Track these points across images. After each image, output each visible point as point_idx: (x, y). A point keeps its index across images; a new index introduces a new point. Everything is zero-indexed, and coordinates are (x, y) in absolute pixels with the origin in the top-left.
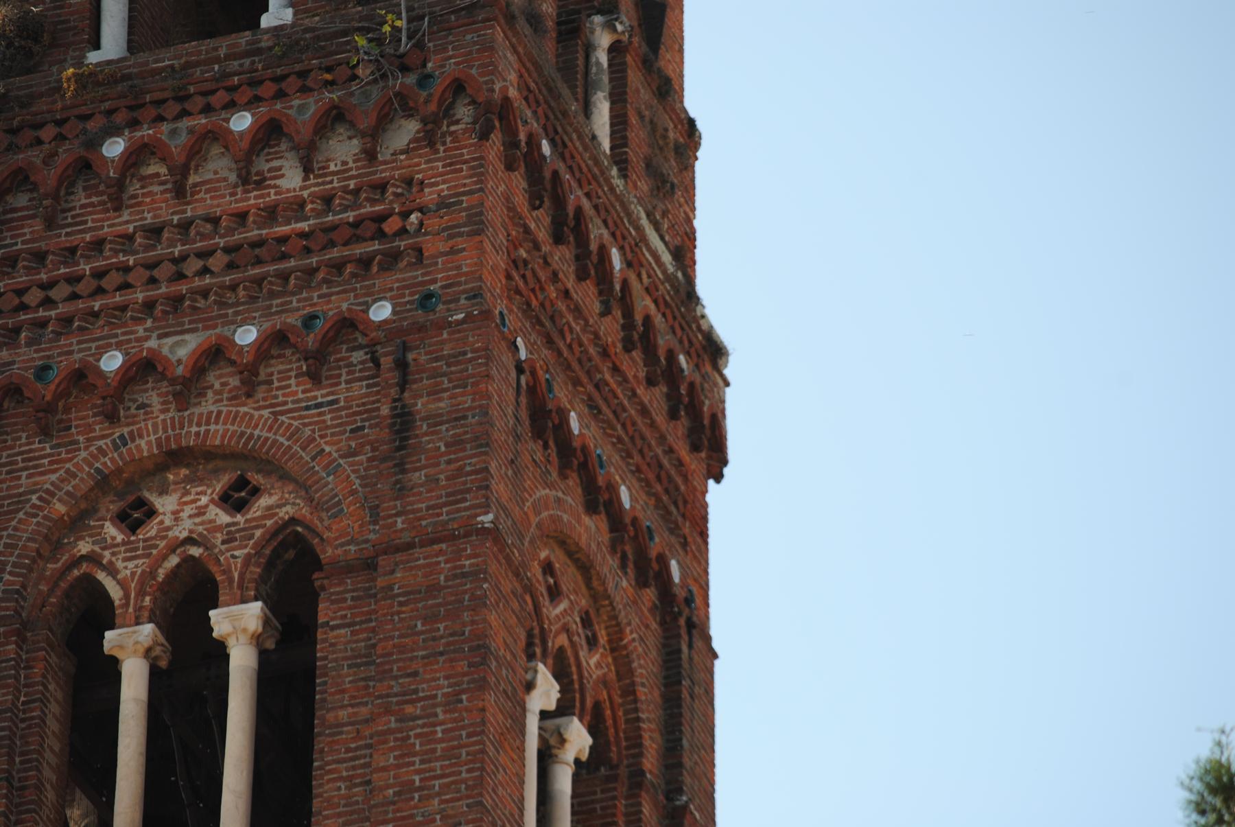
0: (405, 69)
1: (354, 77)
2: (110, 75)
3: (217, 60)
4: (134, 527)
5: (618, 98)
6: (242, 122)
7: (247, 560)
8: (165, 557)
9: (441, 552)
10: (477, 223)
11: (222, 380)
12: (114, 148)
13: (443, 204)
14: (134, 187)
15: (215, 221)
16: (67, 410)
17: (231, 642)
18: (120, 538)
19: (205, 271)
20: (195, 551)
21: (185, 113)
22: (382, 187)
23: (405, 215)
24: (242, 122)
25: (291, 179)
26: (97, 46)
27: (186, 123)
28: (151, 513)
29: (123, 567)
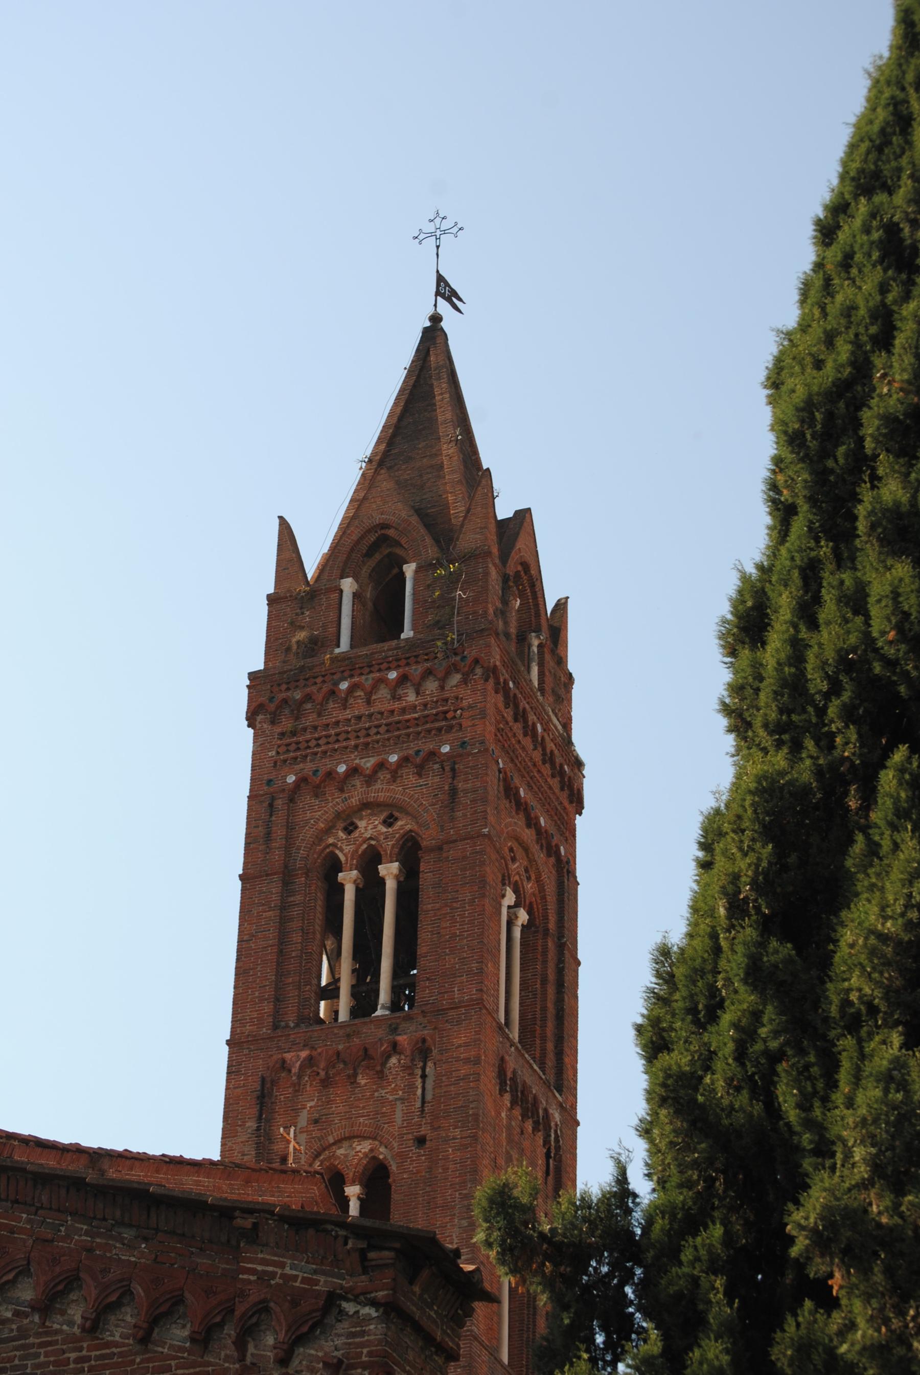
0: (456, 654)
1: (436, 657)
2: (344, 657)
3: (384, 651)
4: (350, 833)
5: (541, 665)
6: (393, 675)
7: (393, 846)
8: (361, 845)
9: (468, 844)
10: (483, 714)
11: (384, 775)
12: (344, 686)
13: (470, 707)
14: (351, 701)
15: (382, 713)
16: (325, 787)
17: (387, 878)
18: (344, 837)
19: (378, 733)
20: (373, 842)
21: (371, 672)
22: (446, 700)
23: (455, 711)
24: (393, 675)
25: (411, 697)
26: (339, 646)
27: (371, 676)
28: (356, 827)
29: (346, 849)
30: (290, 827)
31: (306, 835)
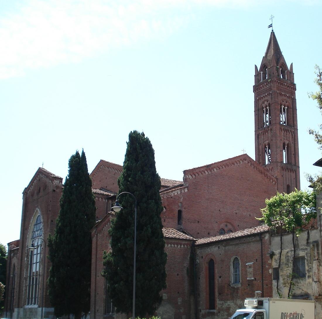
11: (266, 96)
12: (261, 86)
30: (258, 104)
31: (260, 105)
